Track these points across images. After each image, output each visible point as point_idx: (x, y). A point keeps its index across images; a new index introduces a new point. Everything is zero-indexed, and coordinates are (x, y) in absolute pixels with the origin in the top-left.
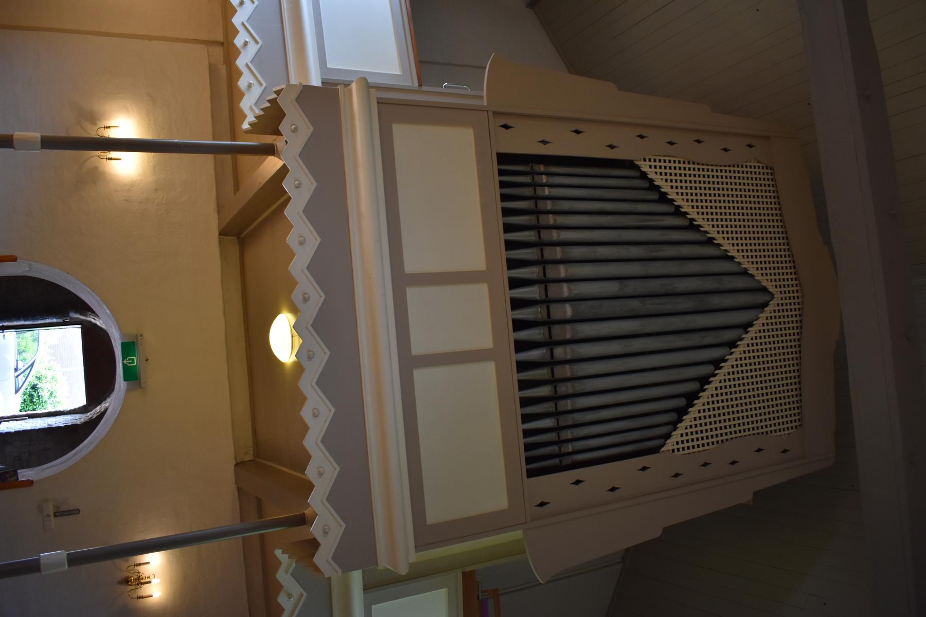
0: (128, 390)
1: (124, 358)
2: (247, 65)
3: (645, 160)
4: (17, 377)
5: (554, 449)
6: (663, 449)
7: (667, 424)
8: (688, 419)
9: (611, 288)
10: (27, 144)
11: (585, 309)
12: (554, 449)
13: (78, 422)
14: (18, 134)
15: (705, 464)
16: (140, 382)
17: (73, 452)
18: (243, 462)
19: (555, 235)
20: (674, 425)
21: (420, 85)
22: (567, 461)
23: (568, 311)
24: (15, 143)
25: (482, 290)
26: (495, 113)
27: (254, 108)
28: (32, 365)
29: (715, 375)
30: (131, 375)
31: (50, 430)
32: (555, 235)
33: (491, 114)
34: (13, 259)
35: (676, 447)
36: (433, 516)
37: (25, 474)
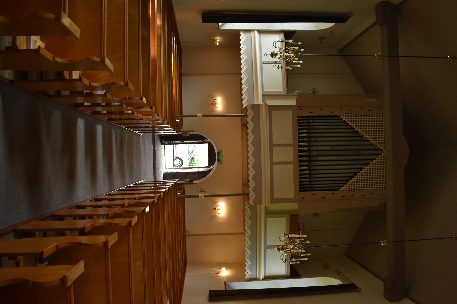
0: (218, 164)
1: (217, 156)
2: (245, 93)
3: (342, 115)
4: (188, 155)
5: (309, 186)
6: (340, 190)
7: (343, 183)
8: (349, 183)
9: (329, 148)
10: (199, 116)
11: (320, 153)
12: (309, 186)
13: (206, 171)
14: (198, 115)
15: (353, 195)
16: (221, 162)
17: (205, 178)
18: (244, 184)
19: (313, 135)
20: (345, 184)
21: (287, 93)
22: (312, 189)
23: (315, 153)
24: (197, 116)
25: (291, 148)
26: (298, 107)
27: (246, 103)
28: (193, 152)
29: (360, 172)
30: (219, 160)
31: (199, 172)
32: (313, 135)
33: (297, 107)
34: (194, 131)
35: (344, 189)
36: (276, 196)
37: (194, 182)
